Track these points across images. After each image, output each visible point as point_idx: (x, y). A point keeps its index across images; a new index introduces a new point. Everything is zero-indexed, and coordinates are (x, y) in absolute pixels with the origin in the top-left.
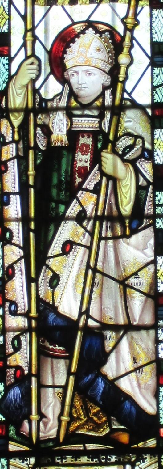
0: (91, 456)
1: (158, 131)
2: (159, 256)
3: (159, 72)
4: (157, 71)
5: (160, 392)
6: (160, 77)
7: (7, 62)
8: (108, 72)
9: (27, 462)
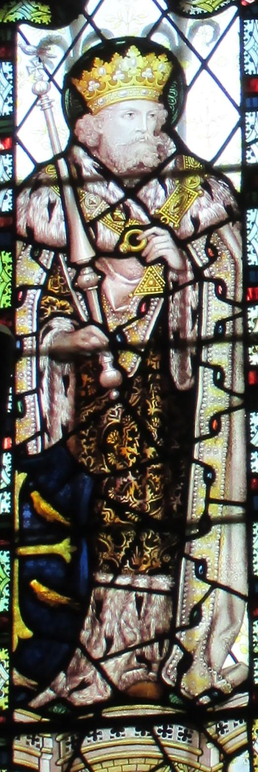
3: (254, 28)
4: (250, 26)
5: (249, 354)
7: (10, 260)
9: (38, 743)
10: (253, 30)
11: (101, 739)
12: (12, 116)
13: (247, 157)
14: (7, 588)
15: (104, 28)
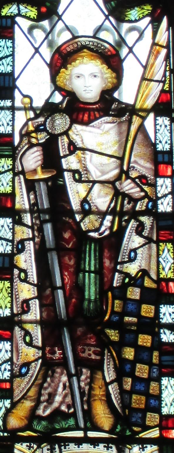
0: (74, 284)
6: (6, 62)
10: (170, 407)
11: (69, 448)
12: (12, 74)
13: (162, 388)
14: (11, 62)
15: (70, 25)
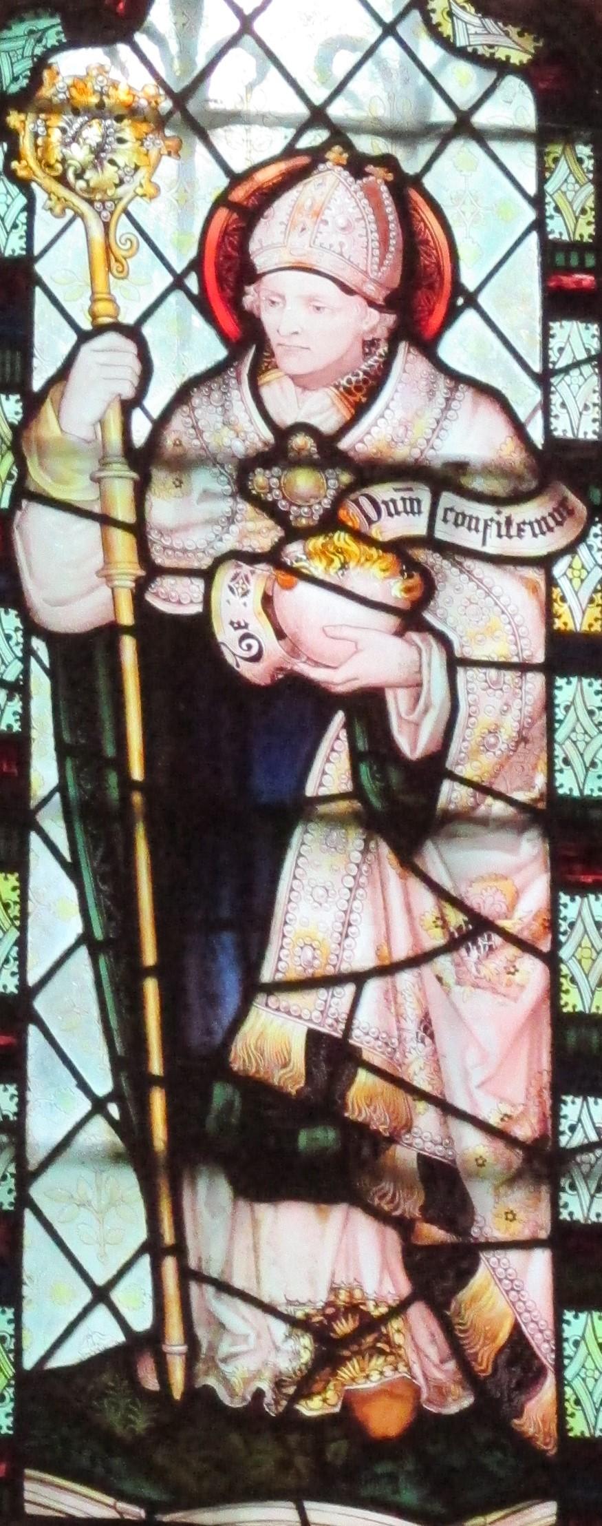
1: (585, 433)
2: (562, 676)
8: (381, 302)
